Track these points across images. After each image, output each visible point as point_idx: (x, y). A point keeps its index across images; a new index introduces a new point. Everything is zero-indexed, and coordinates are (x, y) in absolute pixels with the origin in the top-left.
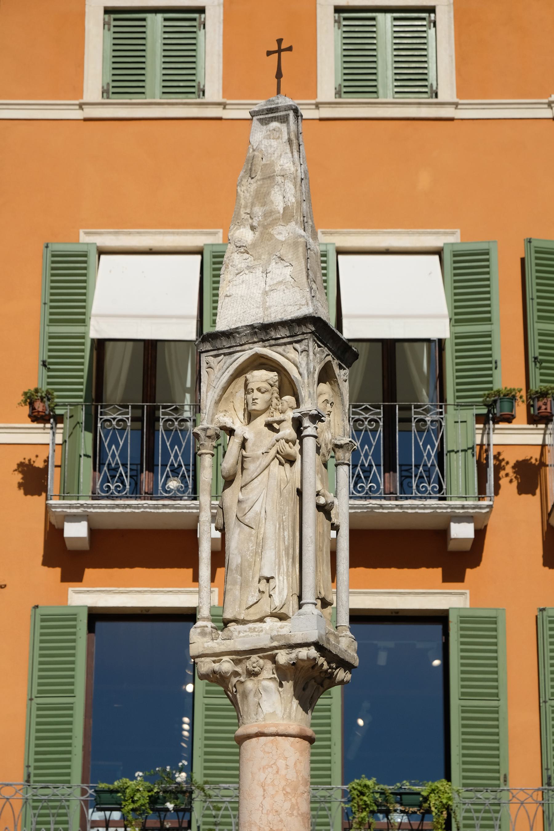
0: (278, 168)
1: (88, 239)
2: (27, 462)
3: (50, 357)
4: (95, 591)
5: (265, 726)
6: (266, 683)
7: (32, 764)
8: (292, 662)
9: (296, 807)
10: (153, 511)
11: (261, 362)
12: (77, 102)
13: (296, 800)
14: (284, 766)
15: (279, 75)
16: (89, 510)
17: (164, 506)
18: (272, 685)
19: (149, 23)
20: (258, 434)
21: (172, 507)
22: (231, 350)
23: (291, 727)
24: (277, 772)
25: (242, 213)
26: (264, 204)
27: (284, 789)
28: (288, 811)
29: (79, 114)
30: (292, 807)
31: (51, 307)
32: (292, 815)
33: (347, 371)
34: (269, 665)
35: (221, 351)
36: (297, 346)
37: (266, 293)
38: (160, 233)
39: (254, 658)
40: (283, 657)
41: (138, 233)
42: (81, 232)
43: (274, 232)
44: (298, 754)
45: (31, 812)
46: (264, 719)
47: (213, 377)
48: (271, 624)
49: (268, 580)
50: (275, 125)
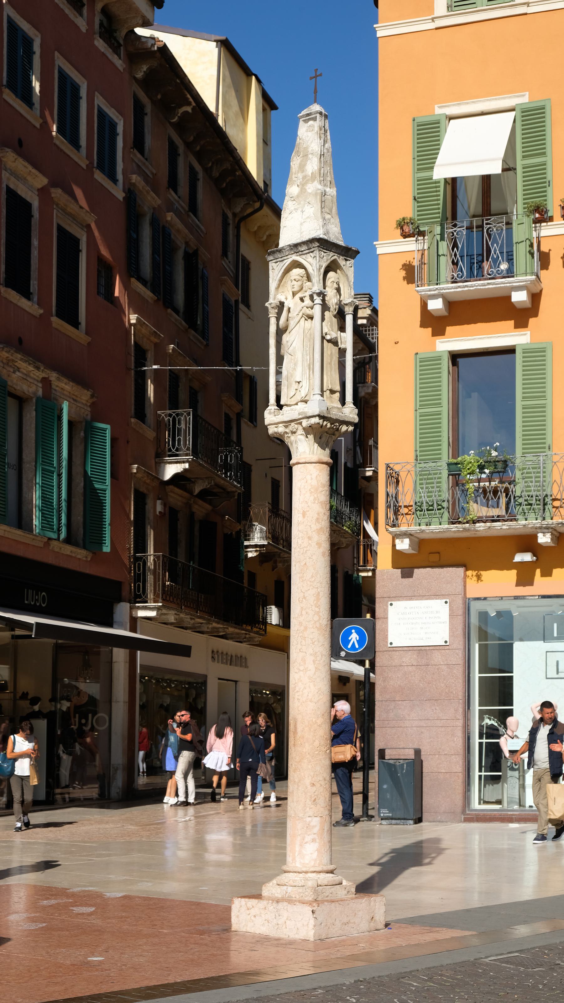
0: (310, 150)
1: (439, 111)
2: (408, 263)
3: (418, 194)
4: (453, 341)
5: (300, 459)
7: (418, 449)
10: (482, 287)
11: (297, 265)
12: (430, 17)
15: (316, 92)
16: (442, 291)
17: (488, 284)
18: (303, 438)
20: (296, 304)
21: (494, 284)
22: (282, 259)
25: (293, 177)
26: (303, 172)
29: (432, 26)
30: (315, 499)
31: (418, 161)
33: (352, 261)
34: (300, 428)
35: (278, 260)
36: (311, 254)
37: (301, 224)
38: (488, 100)
39: (293, 424)
40: (305, 423)
41: (473, 102)
42: (436, 106)
43: (307, 188)
44: (318, 472)
45: (419, 477)
46: (300, 455)
47: (275, 274)
48: (301, 405)
49: (299, 383)
50: (311, 122)
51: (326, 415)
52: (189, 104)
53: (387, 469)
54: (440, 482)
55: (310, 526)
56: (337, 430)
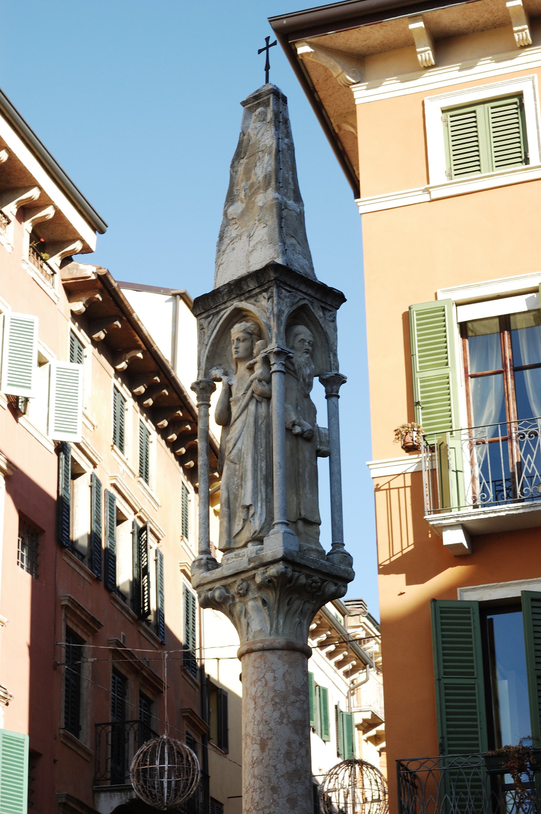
6: (250, 604)
8: (267, 580)
9: (286, 716)
11: (239, 315)
13: (286, 709)
14: (273, 678)
15: (267, 68)
19: (478, 114)
23: (277, 641)
24: (266, 684)
27: (272, 700)
28: (277, 720)
30: (282, 716)
32: (281, 723)
36: (264, 294)
44: (287, 666)
51: (298, 560)
52: (138, 348)
53: (398, 769)
54: (479, 787)
55: (275, 766)
56: (319, 589)
